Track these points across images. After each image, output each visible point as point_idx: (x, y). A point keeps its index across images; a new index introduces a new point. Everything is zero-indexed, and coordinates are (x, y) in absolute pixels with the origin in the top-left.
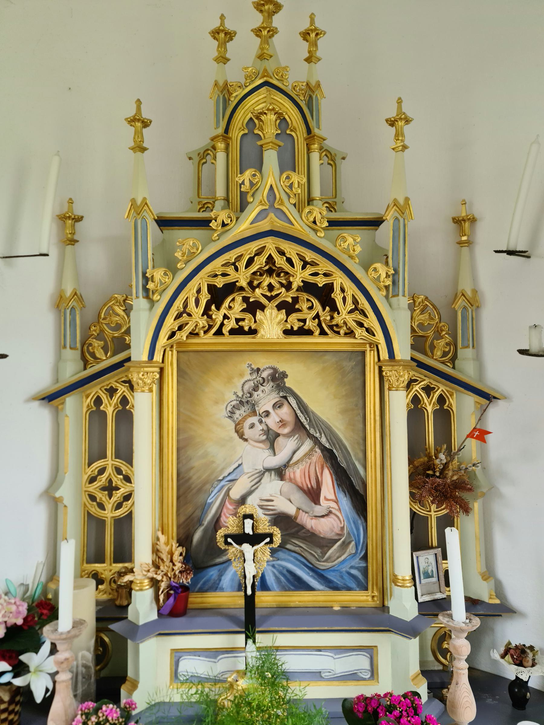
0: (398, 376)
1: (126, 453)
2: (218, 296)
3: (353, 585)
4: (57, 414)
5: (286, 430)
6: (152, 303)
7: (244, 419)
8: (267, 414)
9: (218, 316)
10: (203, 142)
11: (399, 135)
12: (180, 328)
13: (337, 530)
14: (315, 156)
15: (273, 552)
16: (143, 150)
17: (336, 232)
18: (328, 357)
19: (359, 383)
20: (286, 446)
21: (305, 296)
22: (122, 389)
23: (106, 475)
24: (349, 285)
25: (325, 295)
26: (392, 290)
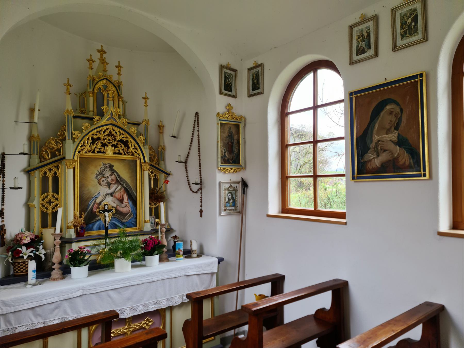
0: (146, 167)
2: (94, 141)
3: (132, 226)
5: (114, 182)
6: (74, 142)
7: (101, 179)
8: (108, 177)
11: (146, 102)
12: (82, 150)
15: (113, 215)
18: (126, 161)
20: (114, 187)
22: (55, 169)
24: (133, 141)
25: (126, 143)
26: (145, 144)
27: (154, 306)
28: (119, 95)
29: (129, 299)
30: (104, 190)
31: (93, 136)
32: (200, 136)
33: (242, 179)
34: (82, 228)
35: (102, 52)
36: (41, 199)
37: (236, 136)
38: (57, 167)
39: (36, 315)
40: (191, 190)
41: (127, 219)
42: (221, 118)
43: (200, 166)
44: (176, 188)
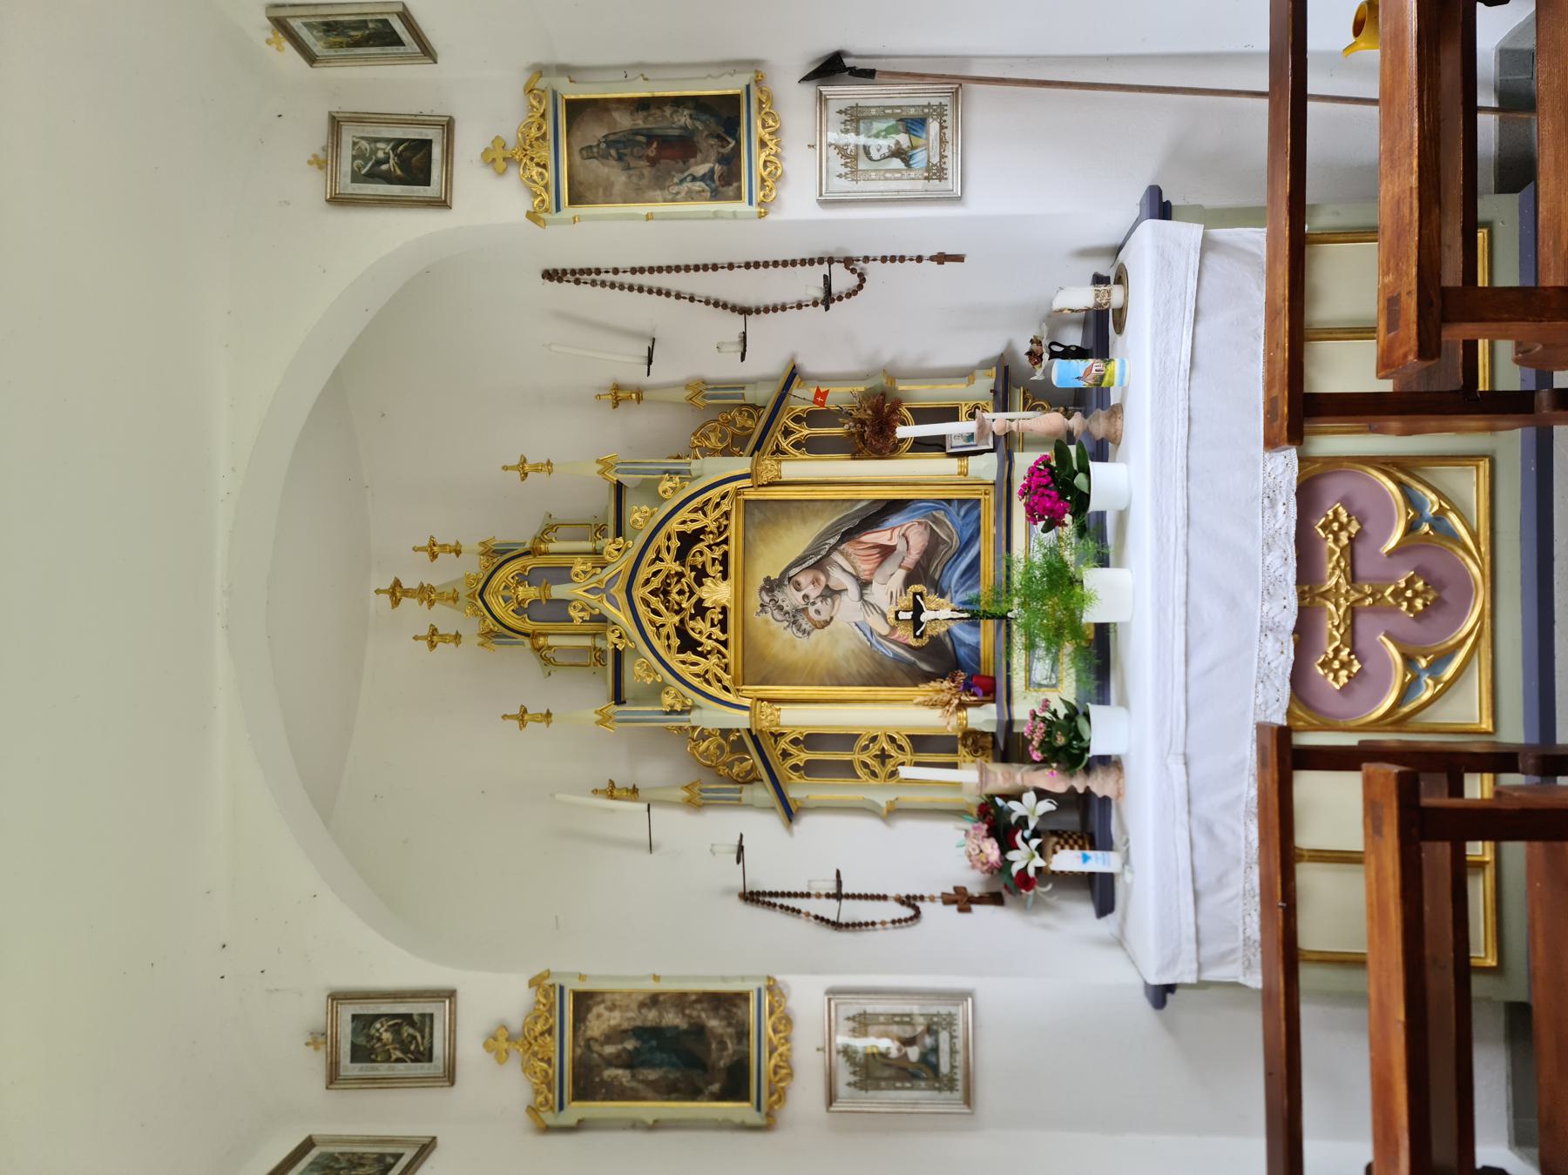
0: (768, 467)
1: (847, 740)
2: (688, 644)
3: (975, 514)
4: (806, 809)
5: (823, 578)
6: (695, 707)
7: (810, 619)
8: (806, 597)
9: (709, 645)
10: (533, 659)
12: (720, 681)
13: (921, 529)
14: (552, 547)
16: (549, 714)
17: (627, 528)
18: (750, 536)
19: (776, 506)
20: (838, 578)
21: (689, 558)
22: (783, 744)
23: (869, 761)
24: (678, 517)
25: (689, 540)
27: (1281, 508)
28: (527, 553)
29: (1233, 603)
30: (848, 608)
31: (674, 649)
32: (637, 265)
33: (806, 79)
34: (967, 687)
35: (396, 592)
36: (872, 782)
37: (616, 115)
38: (777, 736)
39: (1221, 882)
40: (855, 293)
41: (950, 531)
42: (549, 198)
43: (757, 265)
44: (839, 350)
